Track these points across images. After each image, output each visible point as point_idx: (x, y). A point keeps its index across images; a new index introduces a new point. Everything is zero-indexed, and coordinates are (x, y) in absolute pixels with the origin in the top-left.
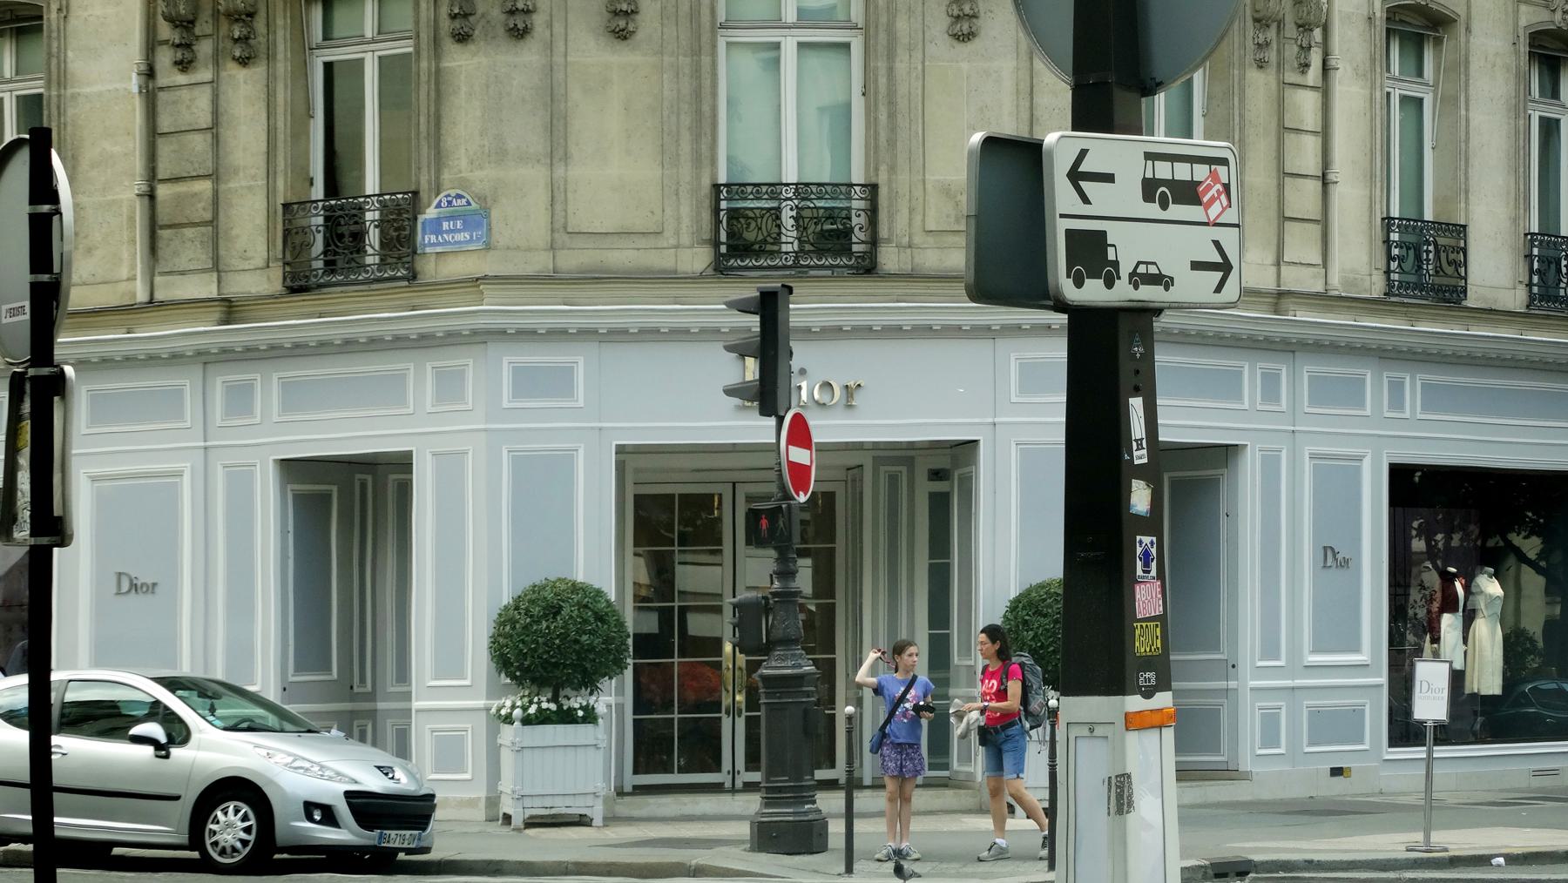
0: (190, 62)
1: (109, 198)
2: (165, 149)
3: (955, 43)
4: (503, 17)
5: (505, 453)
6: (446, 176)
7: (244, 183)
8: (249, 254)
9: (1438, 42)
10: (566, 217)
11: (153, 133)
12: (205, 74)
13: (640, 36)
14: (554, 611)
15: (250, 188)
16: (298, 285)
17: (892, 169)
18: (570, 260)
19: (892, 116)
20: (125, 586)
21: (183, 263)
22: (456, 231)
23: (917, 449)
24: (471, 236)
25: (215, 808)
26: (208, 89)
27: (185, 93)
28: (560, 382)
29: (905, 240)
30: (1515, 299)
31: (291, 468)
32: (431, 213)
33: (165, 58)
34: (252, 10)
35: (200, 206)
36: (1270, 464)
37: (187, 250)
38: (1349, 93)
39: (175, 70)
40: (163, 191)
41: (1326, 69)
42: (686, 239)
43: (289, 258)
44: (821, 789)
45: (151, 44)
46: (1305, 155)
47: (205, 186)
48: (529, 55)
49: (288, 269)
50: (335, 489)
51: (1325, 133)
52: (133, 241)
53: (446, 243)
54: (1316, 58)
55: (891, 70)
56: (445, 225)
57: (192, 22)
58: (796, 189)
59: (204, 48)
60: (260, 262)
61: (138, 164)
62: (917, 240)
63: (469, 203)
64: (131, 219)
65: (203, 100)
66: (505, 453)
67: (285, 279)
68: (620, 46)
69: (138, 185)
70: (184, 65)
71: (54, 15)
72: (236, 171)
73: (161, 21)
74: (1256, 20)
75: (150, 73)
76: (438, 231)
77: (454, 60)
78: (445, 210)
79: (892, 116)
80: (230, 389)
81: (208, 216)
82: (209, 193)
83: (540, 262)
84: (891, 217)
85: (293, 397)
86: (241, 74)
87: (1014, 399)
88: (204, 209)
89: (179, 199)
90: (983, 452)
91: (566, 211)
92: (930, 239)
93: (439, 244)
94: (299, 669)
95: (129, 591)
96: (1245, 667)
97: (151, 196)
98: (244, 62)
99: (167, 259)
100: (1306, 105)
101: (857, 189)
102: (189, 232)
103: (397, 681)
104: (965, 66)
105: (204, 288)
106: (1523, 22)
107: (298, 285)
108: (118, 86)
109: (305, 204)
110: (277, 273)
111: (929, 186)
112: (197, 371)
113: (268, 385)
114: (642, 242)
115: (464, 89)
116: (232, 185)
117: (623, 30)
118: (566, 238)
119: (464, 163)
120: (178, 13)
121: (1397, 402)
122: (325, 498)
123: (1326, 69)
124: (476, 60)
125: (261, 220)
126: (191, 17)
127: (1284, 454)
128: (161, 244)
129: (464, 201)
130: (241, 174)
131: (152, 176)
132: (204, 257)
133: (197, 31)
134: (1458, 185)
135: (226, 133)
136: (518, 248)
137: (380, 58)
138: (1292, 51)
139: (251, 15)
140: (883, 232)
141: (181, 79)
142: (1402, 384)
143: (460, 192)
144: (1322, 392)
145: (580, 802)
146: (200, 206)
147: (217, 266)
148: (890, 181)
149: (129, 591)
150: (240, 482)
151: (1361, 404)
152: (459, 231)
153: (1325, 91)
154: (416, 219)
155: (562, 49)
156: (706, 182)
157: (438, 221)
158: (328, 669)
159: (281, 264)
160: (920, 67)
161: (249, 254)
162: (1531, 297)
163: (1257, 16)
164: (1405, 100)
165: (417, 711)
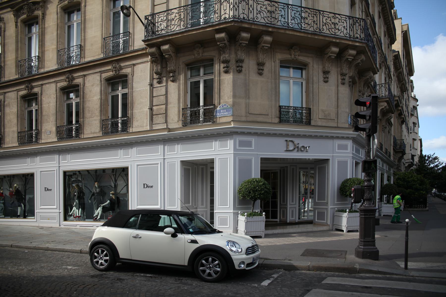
0: (161, 82)
1: (142, 110)
2: (155, 99)
3: (324, 83)
4: (236, 68)
5: (237, 158)
6: (222, 101)
7: (172, 105)
8: (174, 120)
10: (249, 110)
12: (164, 84)
13: (264, 75)
15: (174, 106)
17: (313, 106)
18: (251, 118)
19: (313, 95)
20: (146, 186)
22: (224, 112)
23: (90, 190)
24: (228, 113)
25: (222, 270)
26: (154, 105)
27: (159, 88)
28: (249, 144)
29: (315, 120)
31: (182, 162)
32: (218, 109)
33: (155, 81)
34: (175, 70)
35: (162, 110)
39: (157, 84)
42: (273, 117)
43: (183, 119)
44: (116, 190)
45: (152, 79)
47: (164, 106)
48: (241, 76)
49: (183, 122)
50: (191, 168)
52: (147, 119)
53: (222, 115)
55: (313, 87)
56: (222, 111)
57: (161, 74)
58: (296, 108)
60: (177, 121)
62: (317, 120)
63: (227, 106)
64: (147, 114)
65: (164, 89)
66: (237, 158)
67: (182, 124)
68: (260, 76)
70: (159, 83)
71: (130, 76)
72: (171, 103)
73: (154, 74)
74: (359, 91)
75: (151, 85)
76: (220, 112)
77: (224, 77)
78: (221, 108)
79: (313, 95)
81: (164, 112)
82: (165, 108)
83: (244, 119)
84: (313, 115)
86: (172, 84)
87: (337, 151)
88: (163, 111)
89: (157, 109)
90: (331, 161)
91: (249, 109)
92: (319, 120)
93: (220, 115)
95: (146, 187)
98: (173, 81)
99: (155, 121)
101: (305, 108)
102: (160, 116)
103: (202, 205)
104: (326, 87)
108: (144, 88)
110: (180, 123)
111: (320, 110)
114: (264, 116)
115: (226, 83)
116: (169, 106)
117: (261, 73)
118: (249, 115)
119: (226, 98)
120: (158, 72)
122: (189, 169)
124: (229, 77)
125: (176, 112)
126: (161, 73)
129: (226, 106)
130: (172, 104)
132: (163, 120)
133: (162, 76)
135: (169, 96)
136: (239, 116)
137: (204, 80)
139: (175, 72)
140: (312, 118)
141: (159, 85)
143: (225, 104)
145: (259, 233)
146: (162, 110)
147: (166, 122)
148: (313, 108)
149: (146, 187)
152: (225, 112)
154: (214, 110)
155: (248, 76)
156: (278, 105)
157: (220, 110)
158: (189, 203)
159: (181, 121)
160: (318, 87)
161: (174, 120)
163: (359, 90)
165: (215, 213)
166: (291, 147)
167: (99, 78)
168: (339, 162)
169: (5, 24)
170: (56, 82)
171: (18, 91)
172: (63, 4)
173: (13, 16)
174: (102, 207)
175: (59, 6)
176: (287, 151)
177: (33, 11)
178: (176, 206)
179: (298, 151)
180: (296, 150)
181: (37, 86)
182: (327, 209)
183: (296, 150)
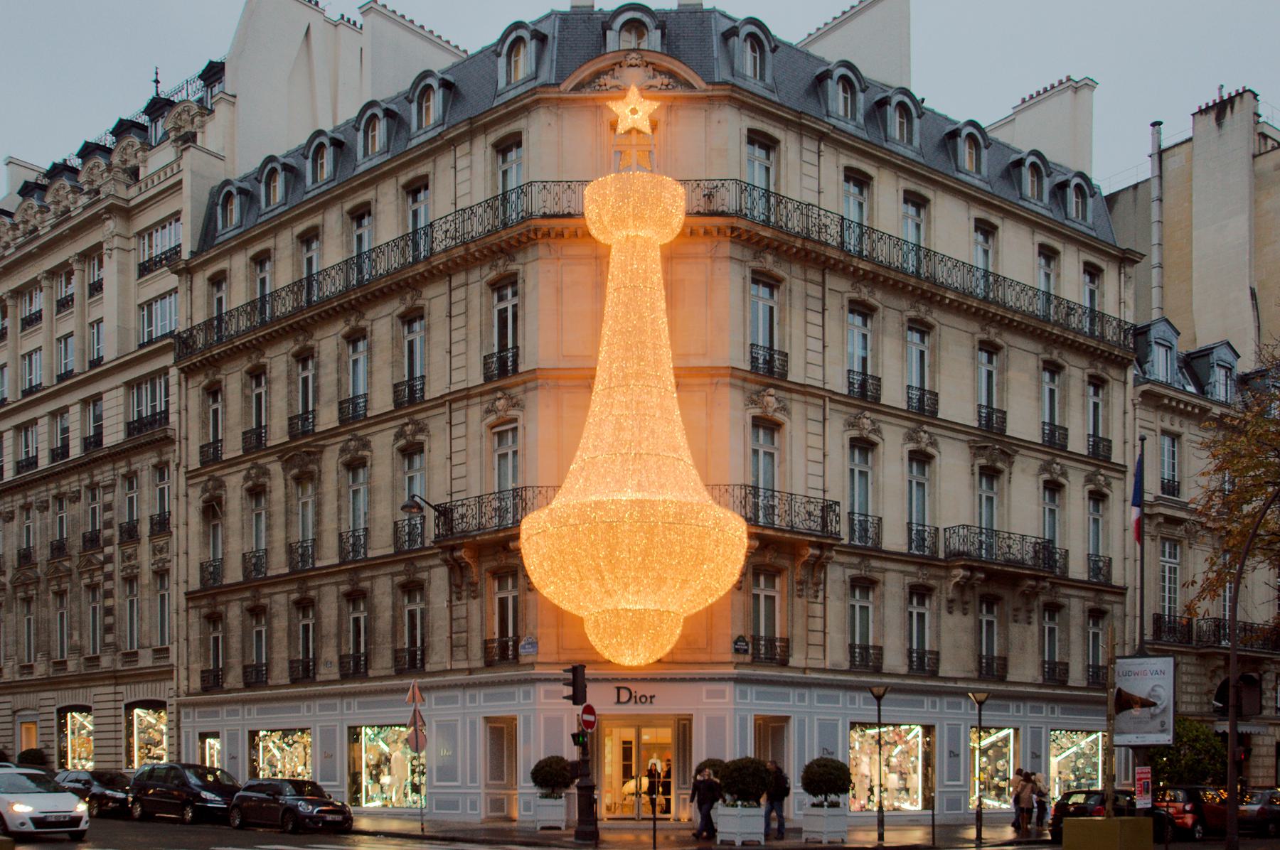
9: (874, 589)
11: (452, 619)
12: (464, 601)
14: (825, 766)
16: (489, 664)
21: (458, 658)
30: (904, 670)
32: (523, 643)
33: (454, 597)
36: (801, 723)
37: (460, 654)
38: (1075, 634)
40: (454, 636)
41: (825, 598)
45: (451, 593)
46: (818, 624)
51: (824, 617)
54: (821, 594)
59: (464, 594)
61: (448, 628)
65: (464, 608)
69: (448, 635)
75: (451, 601)
80: (471, 696)
85: (488, 698)
94: (492, 779)
96: (483, 796)
97: (451, 637)
100: (818, 609)
105: (464, 665)
106: (907, 582)
107: (489, 664)
109: (493, 641)
112: (461, 690)
113: (481, 694)
121: (1053, 712)
123: (825, 598)
127: (840, 723)
128: (455, 653)
131: (451, 633)
134: (881, 634)
138: (811, 592)
142: (746, 692)
144: (1033, 710)
147: (467, 659)
150: (473, 724)
151: (960, 708)
153: (824, 604)
162: (1089, 683)
164: (766, 597)
166: (624, 696)
167: (390, 583)
168: (708, 719)
169: (371, 451)
170: (393, 575)
171: (289, 592)
172: (344, 458)
173: (280, 469)
174: (841, 796)
175: (289, 477)
176: (619, 702)
177: (307, 465)
178: (438, 784)
179: (636, 702)
180: (633, 700)
181: (314, 588)
182: (487, 786)
183: (633, 700)
